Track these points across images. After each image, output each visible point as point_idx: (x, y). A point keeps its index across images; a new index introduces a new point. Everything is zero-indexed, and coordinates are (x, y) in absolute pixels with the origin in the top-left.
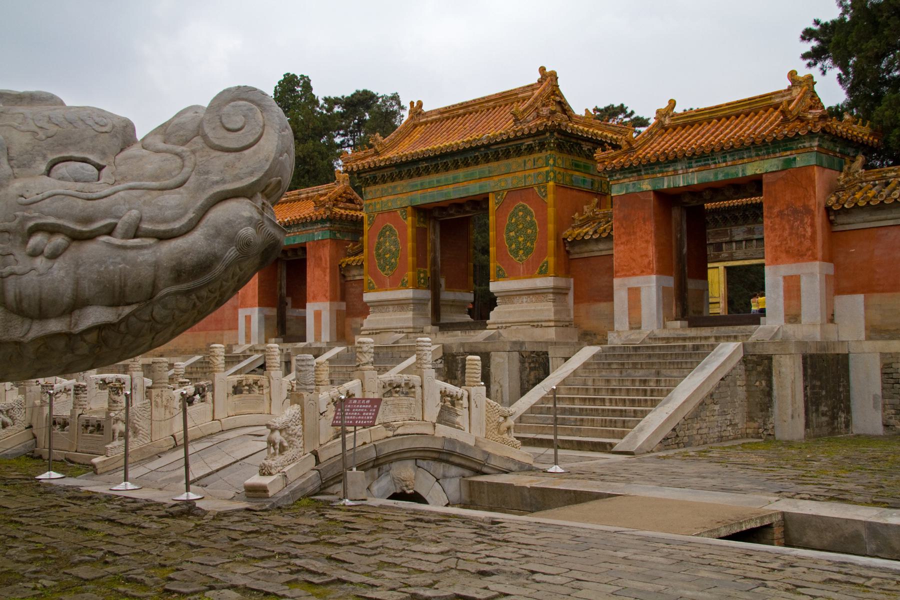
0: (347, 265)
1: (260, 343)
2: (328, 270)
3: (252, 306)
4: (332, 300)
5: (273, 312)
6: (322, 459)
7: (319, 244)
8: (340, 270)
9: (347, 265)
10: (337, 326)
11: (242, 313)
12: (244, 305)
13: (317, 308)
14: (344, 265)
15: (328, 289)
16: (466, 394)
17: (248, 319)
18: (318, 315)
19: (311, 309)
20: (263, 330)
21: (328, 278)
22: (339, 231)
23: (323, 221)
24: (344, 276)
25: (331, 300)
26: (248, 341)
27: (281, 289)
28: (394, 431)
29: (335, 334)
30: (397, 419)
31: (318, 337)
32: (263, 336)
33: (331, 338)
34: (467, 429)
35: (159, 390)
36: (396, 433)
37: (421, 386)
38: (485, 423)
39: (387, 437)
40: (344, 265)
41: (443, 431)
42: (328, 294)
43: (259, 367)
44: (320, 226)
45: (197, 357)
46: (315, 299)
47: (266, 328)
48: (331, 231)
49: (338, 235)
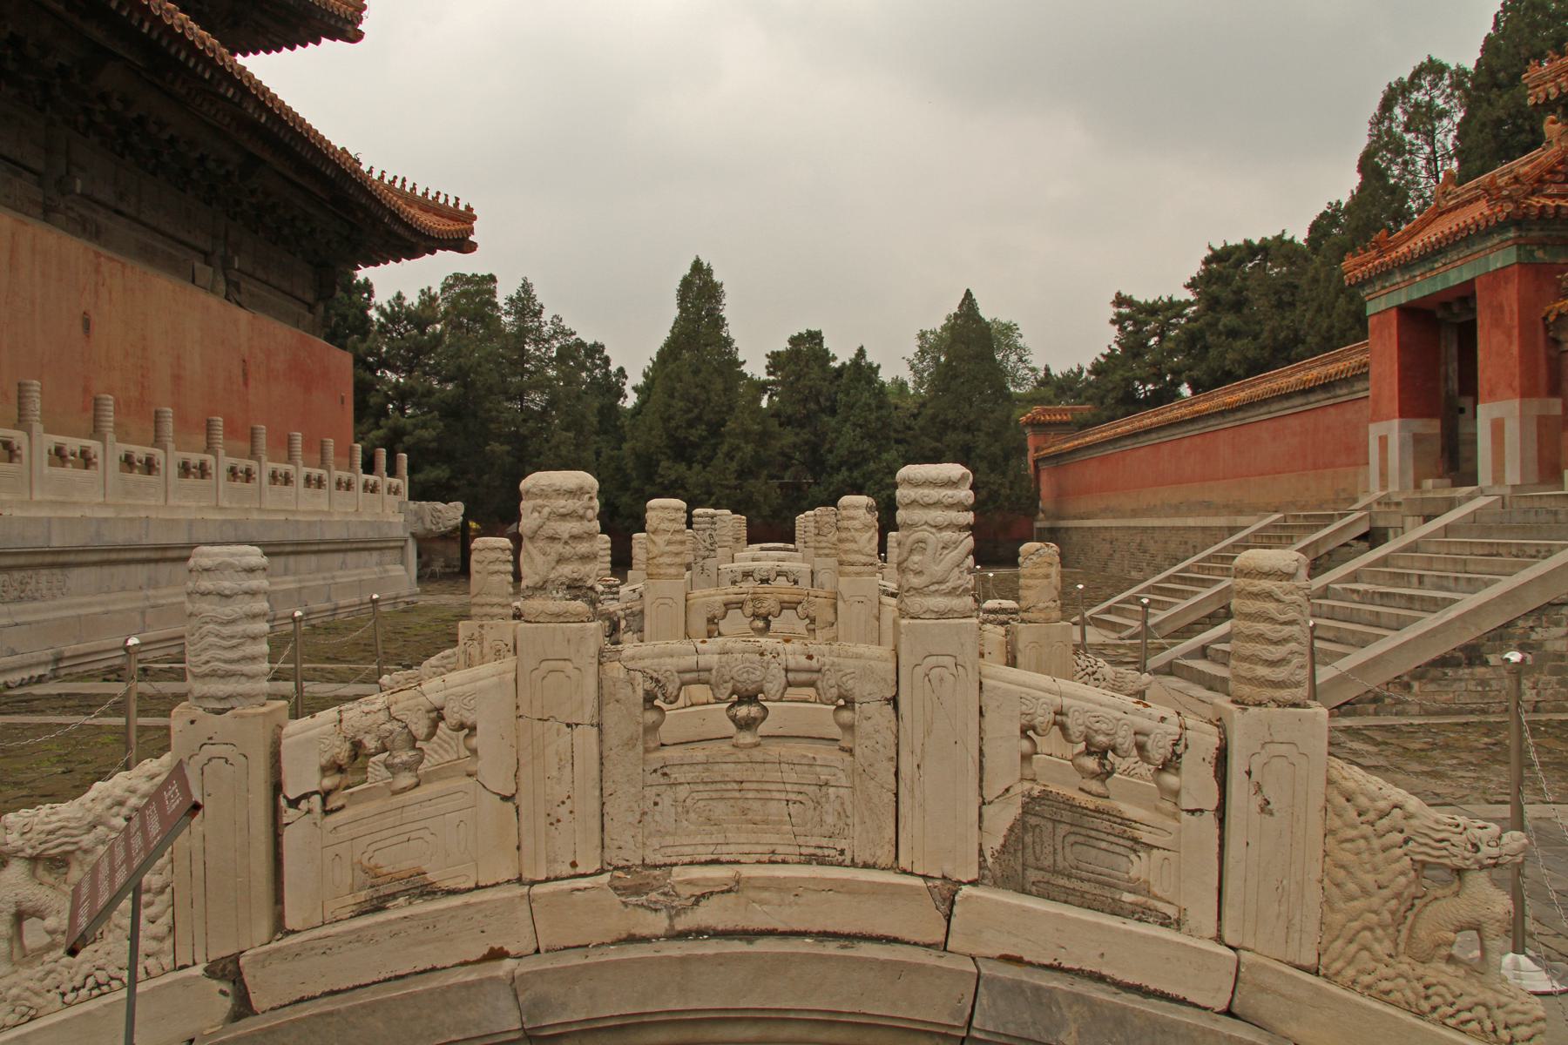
0: (1560, 316)
1: (1403, 489)
2: (1516, 332)
3: (1389, 418)
4: (1526, 393)
5: (1433, 427)
6: (259, 1000)
7: (1499, 275)
8: (1547, 329)
9: (1560, 316)
10: (1540, 451)
11: (1375, 431)
12: (1377, 417)
13: (1496, 414)
14: (1551, 318)
15: (1517, 371)
16: (1209, 740)
17: (1383, 441)
18: (1498, 427)
19: (1486, 413)
20: (1410, 463)
21: (1515, 349)
22: (1542, 245)
23: (1501, 227)
24: (1556, 342)
25: (1523, 395)
26: (1384, 486)
27: (1446, 380)
28: (674, 913)
29: (1533, 467)
30: (726, 853)
31: (1498, 477)
32: (1411, 473)
33: (1522, 476)
34: (1202, 915)
35: (474, 623)
36: (682, 924)
37: (599, 726)
38: (1314, 895)
39: (632, 939)
40: (1551, 318)
41: (1008, 920)
42: (1516, 383)
43: (1358, 538)
44: (1496, 239)
45: (1277, 516)
46: (1492, 395)
47: (1416, 459)
48: (1519, 247)
49: (1539, 254)
